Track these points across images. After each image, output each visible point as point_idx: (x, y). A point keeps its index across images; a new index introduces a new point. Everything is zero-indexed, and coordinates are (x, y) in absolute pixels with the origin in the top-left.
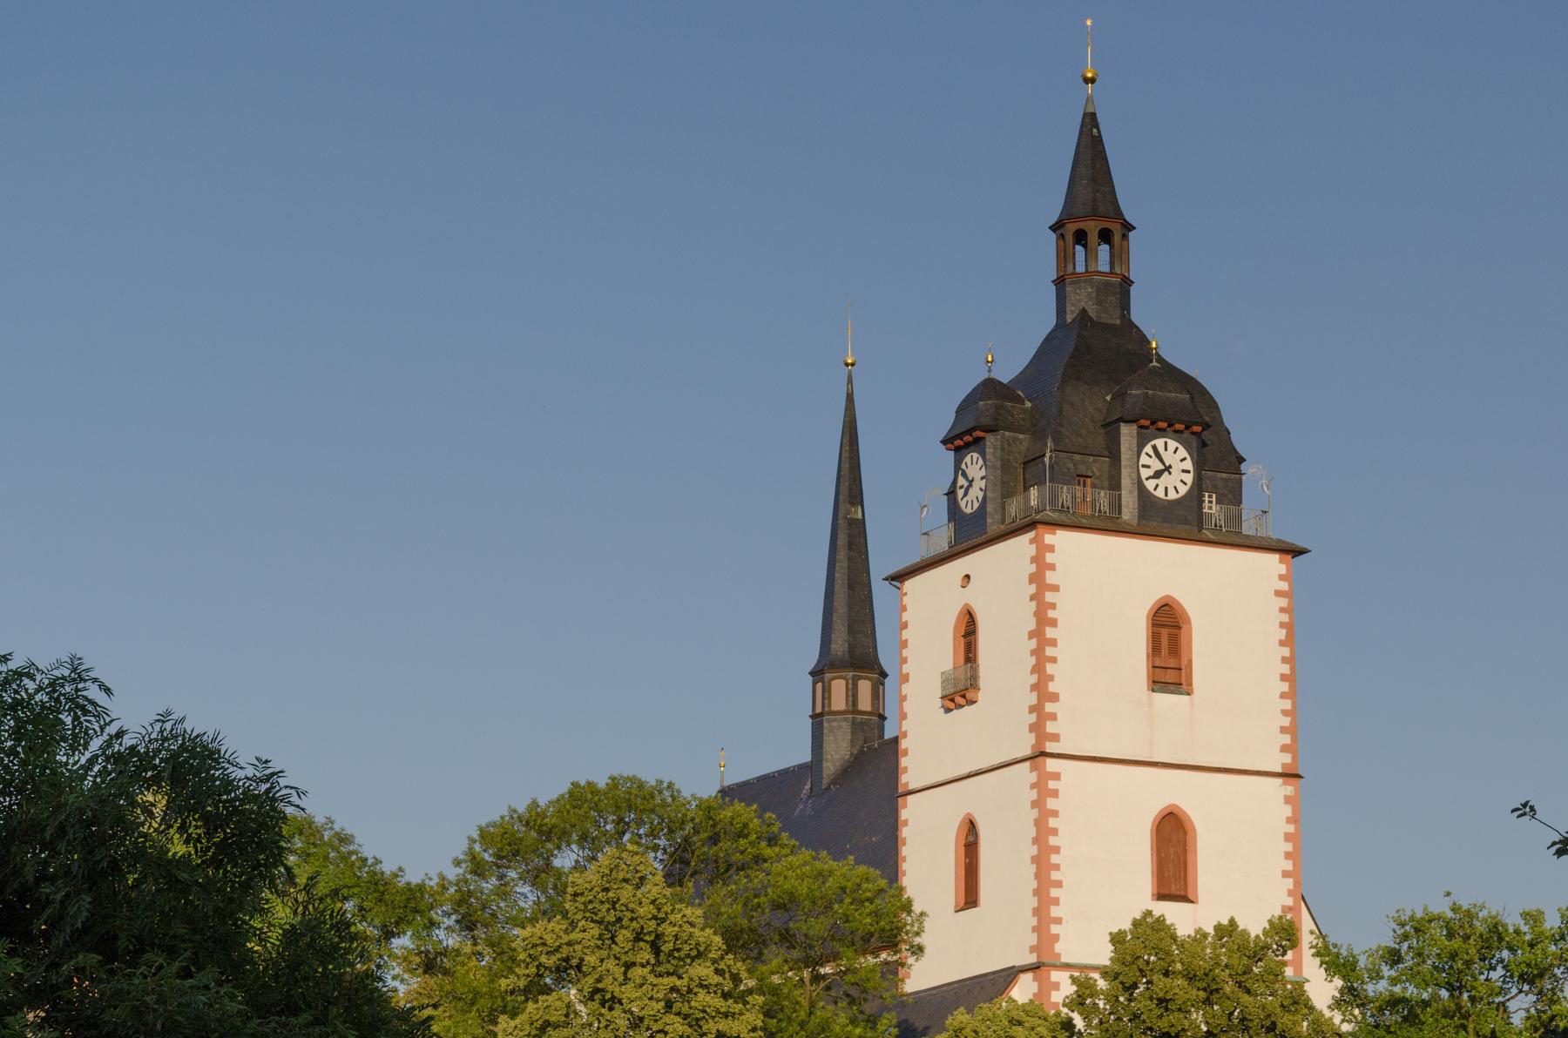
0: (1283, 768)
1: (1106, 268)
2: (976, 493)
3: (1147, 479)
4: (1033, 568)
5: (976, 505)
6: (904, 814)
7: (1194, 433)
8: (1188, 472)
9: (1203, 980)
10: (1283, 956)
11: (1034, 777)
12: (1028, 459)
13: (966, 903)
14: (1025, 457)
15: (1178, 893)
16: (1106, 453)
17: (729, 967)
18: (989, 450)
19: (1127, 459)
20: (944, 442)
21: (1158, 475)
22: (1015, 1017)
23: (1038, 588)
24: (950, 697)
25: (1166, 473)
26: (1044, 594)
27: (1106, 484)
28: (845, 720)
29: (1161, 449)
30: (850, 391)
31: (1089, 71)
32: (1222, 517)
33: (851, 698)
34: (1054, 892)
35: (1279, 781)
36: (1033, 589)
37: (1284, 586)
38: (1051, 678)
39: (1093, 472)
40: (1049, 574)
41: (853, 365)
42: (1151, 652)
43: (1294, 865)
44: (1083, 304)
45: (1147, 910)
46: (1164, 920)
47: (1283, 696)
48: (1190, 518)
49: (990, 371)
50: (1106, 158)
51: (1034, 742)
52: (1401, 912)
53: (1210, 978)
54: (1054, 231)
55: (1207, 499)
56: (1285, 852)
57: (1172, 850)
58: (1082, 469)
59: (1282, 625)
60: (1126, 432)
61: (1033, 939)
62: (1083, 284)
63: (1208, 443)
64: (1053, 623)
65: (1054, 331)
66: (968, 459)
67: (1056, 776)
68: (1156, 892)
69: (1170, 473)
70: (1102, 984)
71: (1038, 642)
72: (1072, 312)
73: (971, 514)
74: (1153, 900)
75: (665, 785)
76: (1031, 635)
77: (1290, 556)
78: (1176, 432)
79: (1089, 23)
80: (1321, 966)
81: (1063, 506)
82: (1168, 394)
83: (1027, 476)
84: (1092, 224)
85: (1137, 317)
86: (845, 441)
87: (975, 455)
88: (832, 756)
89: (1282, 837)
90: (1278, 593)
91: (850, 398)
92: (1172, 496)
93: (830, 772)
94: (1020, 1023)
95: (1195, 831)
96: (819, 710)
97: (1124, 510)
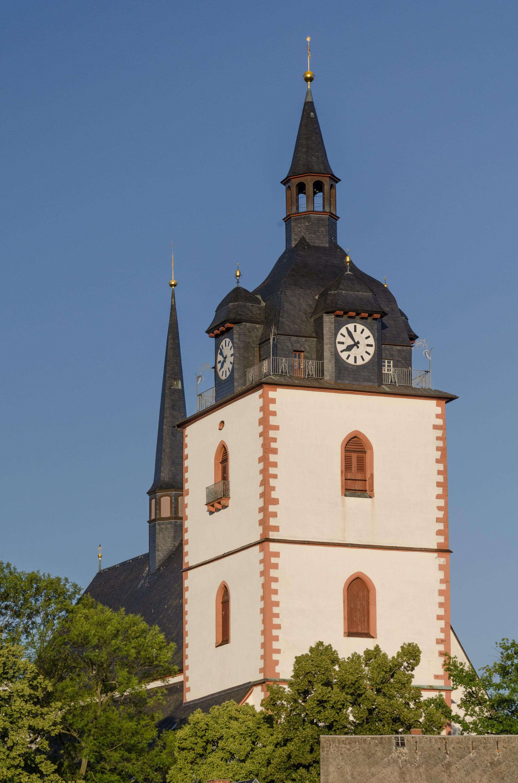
0: (438, 546)
1: (321, 209)
2: (228, 366)
3: (342, 351)
4: (261, 415)
5: (228, 374)
6: (187, 583)
7: (375, 319)
8: (371, 346)
9: (352, 687)
10: (412, 671)
11: (261, 556)
12: (263, 341)
13: (222, 641)
14: (261, 339)
15: (363, 632)
16: (314, 335)
17: (40, 684)
18: (236, 336)
19: (327, 338)
20: (208, 332)
21: (349, 348)
22: (233, 715)
23: (264, 428)
24: (211, 504)
25: (355, 347)
26: (269, 432)
27: (314, 356)
28: (170, 523)
29: (352, 330)
30: (173, 304)
31: (308, 73)
32: (313, 369)
33: (173, 509)
34: (275, 632)
35: (436, 555)
36: (261, 429)
37: (440, 422)
38: (273, 488)
39: (305, 348)
40: (271, 418)
41: (175, 285)
42: (344, 469)
43: (445, 611)
44: (303, 234)
45: (319, 642)
46: (331, 648)
47: (438, 497)
48: (372, 377)
49: (238, 282)
50: (320, 132)
51: (261, 532)
52: (505, 640)
53: (356, 686)
54: (284, 184)
55: (386, 364)
56: (439, 603)
57: (359, 603)
58: (297, 347)
59: (438, 449)
60: (327, 319)
61: (261, 664)
62: (303, 220)
63: (388, 325)
64: (275, 451)
65: (284, 253)
66: (223, 343)
67: (277, 555)
68: (347, 631)
69: (358, 347)
70: (287, 689)
71: (264, 464)
72: (295, 239)
73: (225, 380)
74: (344, 636)
75: (5, 565)
76: (261, 460)
77: (444, 402)
78: (362, 318)
79: (308, 39)
80: (449, 678)
81: (309, 375)
82: (357, 293)
83: (261, 353)
84: (309, 178)
85: (341, 242)
86: (170, 337)
87: (228, 340)
88: (161, 547)
89: (437, 593)
90: (435, 427)
91: (173, 308)
92: (360, 362)
93: (160, 558)
94: (236, 719)
95: (375, 590)
96: (153, 517)
97: (325, 373)
